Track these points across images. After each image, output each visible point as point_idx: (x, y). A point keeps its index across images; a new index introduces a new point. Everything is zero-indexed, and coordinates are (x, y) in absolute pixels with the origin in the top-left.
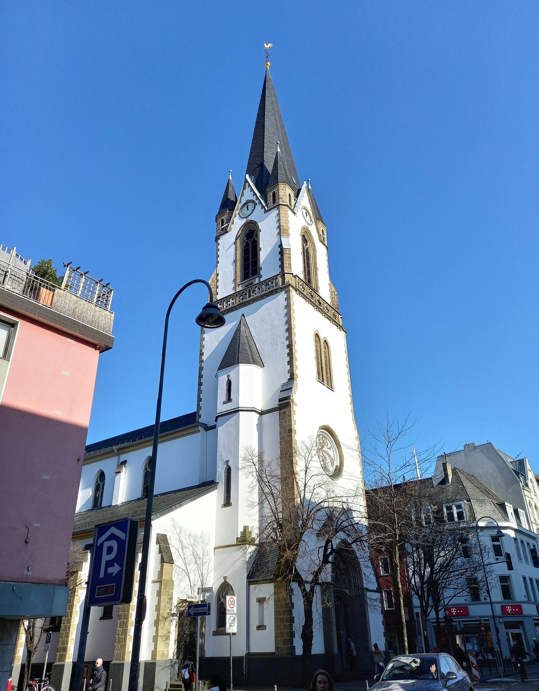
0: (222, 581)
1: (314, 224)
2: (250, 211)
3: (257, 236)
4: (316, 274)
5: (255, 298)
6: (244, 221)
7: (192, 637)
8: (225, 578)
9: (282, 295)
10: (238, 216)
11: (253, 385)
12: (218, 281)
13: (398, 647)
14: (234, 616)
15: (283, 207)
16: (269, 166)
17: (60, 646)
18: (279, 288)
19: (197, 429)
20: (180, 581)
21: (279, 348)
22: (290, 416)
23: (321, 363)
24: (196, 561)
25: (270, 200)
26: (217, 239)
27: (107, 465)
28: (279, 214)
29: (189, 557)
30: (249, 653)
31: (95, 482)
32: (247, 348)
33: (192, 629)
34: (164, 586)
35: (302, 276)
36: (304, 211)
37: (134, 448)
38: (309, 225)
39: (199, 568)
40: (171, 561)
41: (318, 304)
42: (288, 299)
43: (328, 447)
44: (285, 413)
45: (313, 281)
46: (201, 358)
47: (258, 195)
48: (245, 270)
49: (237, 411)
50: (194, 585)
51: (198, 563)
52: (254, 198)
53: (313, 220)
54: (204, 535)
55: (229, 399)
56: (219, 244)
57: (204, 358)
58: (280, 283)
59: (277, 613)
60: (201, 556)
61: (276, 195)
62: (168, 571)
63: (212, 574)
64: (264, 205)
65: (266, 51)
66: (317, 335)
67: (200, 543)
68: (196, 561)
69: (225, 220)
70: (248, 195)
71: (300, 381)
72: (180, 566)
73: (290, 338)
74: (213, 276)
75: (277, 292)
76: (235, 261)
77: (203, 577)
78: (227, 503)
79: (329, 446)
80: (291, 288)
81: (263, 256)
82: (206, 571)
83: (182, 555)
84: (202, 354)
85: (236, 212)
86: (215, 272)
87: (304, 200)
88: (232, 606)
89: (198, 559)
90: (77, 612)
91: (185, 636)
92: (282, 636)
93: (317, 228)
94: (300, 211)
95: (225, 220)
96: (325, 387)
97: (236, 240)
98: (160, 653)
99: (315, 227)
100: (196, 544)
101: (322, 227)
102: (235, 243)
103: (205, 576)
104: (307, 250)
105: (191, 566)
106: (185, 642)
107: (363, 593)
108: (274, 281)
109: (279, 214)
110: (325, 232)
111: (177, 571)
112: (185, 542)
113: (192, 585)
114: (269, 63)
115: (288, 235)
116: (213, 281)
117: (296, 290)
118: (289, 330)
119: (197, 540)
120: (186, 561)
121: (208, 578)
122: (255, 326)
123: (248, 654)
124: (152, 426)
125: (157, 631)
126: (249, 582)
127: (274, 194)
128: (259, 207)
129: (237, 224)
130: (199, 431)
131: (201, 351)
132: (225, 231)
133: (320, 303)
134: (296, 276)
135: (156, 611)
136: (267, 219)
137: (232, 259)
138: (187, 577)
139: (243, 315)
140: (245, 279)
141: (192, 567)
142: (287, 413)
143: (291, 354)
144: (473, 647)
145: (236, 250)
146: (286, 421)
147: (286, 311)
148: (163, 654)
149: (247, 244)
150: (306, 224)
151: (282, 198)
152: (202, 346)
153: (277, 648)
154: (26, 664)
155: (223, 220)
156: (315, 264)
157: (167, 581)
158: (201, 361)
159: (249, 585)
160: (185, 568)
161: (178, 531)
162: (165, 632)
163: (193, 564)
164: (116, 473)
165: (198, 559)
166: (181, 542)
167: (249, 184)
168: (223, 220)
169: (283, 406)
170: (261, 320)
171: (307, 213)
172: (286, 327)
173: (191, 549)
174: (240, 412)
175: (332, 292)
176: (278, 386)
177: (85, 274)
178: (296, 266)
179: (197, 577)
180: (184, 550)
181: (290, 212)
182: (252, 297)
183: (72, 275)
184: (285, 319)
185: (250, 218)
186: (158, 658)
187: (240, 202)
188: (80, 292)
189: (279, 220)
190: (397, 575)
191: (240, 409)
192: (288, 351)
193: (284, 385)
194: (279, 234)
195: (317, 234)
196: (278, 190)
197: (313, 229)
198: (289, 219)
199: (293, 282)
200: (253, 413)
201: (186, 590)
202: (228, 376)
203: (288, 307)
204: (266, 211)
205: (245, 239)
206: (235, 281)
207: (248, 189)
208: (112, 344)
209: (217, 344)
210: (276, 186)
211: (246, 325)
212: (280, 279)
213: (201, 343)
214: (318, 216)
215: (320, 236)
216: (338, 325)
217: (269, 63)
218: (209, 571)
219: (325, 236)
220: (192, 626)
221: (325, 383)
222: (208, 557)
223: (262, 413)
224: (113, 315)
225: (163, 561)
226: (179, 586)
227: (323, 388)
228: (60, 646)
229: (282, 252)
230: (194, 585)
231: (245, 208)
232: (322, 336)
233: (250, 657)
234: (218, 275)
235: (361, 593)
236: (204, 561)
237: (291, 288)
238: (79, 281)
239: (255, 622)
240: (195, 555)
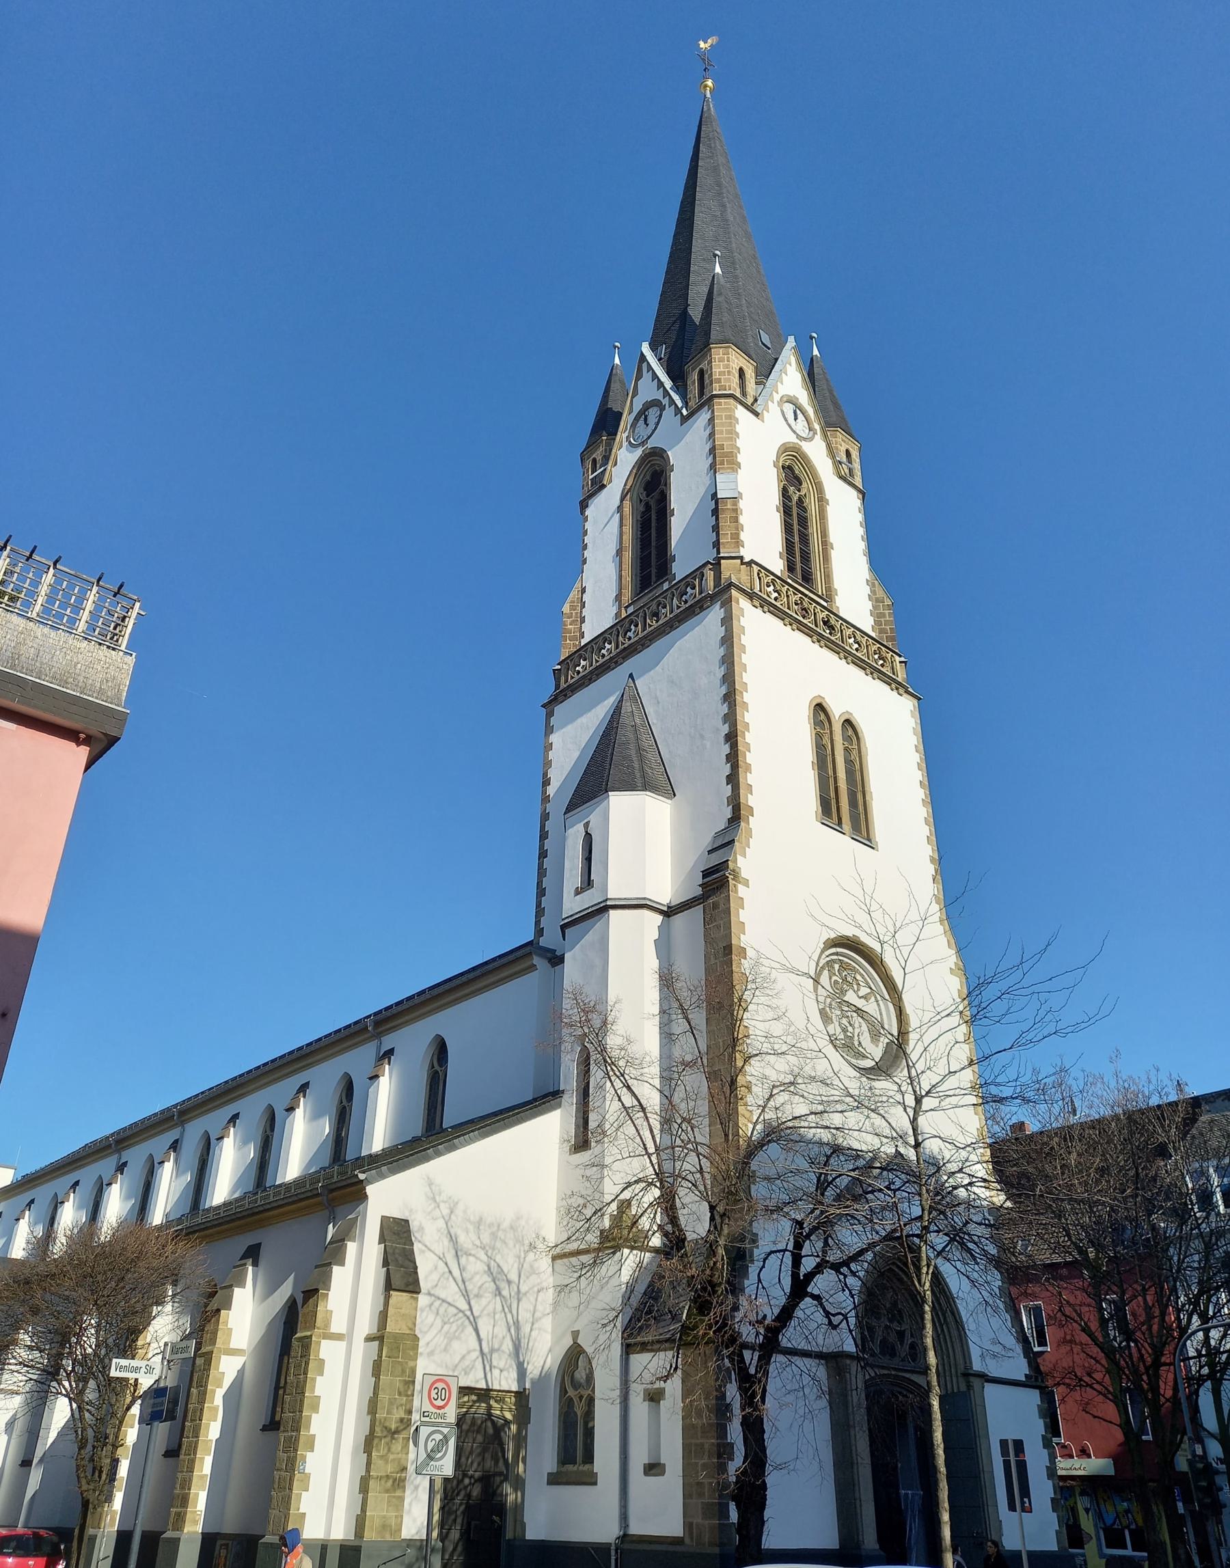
0: (568, 1342)
1: (818, 437)
2: (652, 426)
3: (667, 484)
4: (826, 558)
5: (657, 629)
6: (639, 452)
7: (490, 1484)
8: (576, 1334)
9: (715, 613)
10: (625, 444)
11: (644, 843)
12: (583, 605)
13: (1168, 1542)
14: (445, 1431)
15: (722, 400)
16: (696, 313)
17: (177, 1491)
18: (706, 597)
19: (529, 963)
20: (451, 1340)
21: (708, 744)
22: (728, 911)
23: (835, 778)
24: (498, 1289)
25: (693, 389)
26: (584, 505)
27: (356, 1060)
28: (711, 421)
29: (477, 1278)
30: (625, 1535)
31: (336, 1102)
32: (633, 752)
33: (489, 1464)
34: (390, 1349)
35: (777, 566)
36: (789, 409)
37: (407, 1018)
38: (805, 439)
39: (507, 1308)
40: (412, 1287)
41: (828, 630)
42: (727, 621)
43: (861, 994)
44: (715, 906)
45: (818, 576)
46: (544, 792)
47: (668, 384)
48: (642, 570)
49: (602, 910)
50: (492, 1351)
51: (505, 1293)
52: (659, 395)
53: (817, 427)
54: (523, 1222)
55: (588, 883)
56: (586, 519)
57: (551, 790)
58: (711, 583)
59: (688, 1430)
60: (513, 1276)
61: (706, 376)
62: (403, 1311)
63: (547, 1323)
64: (680, 404)
65: (703, 56)
66: (820, 708)
67: (511, 1243)
68: (498, 1289)
69: (599, 458)
70: (647, 391)
71: (757, 824)
72: (449, 1300)
73: (731, 718)
74: (574, 594)
75: (702, 609)
76: (619, 553)
77: (518, 1328)
78: (582, 1142)
79: (864, 991)
80: (734, 593)
81: (677, 526)
82: (529, 1315)
83: (456, 1273)
84: (546, 782)
85: (622, 435)
86: (578, 585)
87: (790, 379)
88: (439, 1403)
89: (503, 1285)
90: (216, 1409)
91: (467, 1481)
92: (701, 1495)
93: (829, 446)
94: (774, 408)
95: (599, 458)
96: (847, 839)
97: (622, 500)
98: (377, 1522)
99: (824, 444)
100: (498, 1244)
101: (843, 443)
102: (620, 509)
103: (526, 1329)
105: (484, 1301)
106: (469, 1496)
107: (969, 1387)
108: (697, 583)
109: (711, 421)
110: (855, 455)
111: (442, 1311)
112: (464, 1240)
113: (486, 1350)
114: (709, 83)
115: (735, 466)
116: (572, 608)
117: (751, 596)
118: (730, 697)
119: (500, 1234)
120: (469, 1287)
121: (533, 1333)
122: (656, 698)
123: (625, 1537)
125: (369, 1464)
126: (628, 1346)
127: (702, 373)
128: (669, 412)
129: (624, 461)
130: (533, 968)
131: (545, 774)
132: (598, 486)
133: (832, 628)
134: (752, 561)
135: (368, 1413)
136: (688, 438)
137: (613, 547)
138: (470, 1330)
139: (631, 676)
140: (643, 588)
141: (485, 1305)
142: (722, 906)
143: (733, 758)
145: (621, 525)
146: (718, 927)
147: (722, 652)
148: (385, 1527)
149: (648, 507)
150: (792, 439)
151: (719, 381)
152: (548, 764)
153: (688, 1526)
155: (594, 461)
156: (824, 534)
157: (397, 1337)
158: (546, 799)
159: (628, 1354)
160: (465, 1307)
161: (446, 1212)
162: (390, 1469)
163: (488, 1296)
164: (371, 1078)
165: (503, 1285)
166: (453, 1239)
167: (650, 368)
168: (594, 461)
169: (714, 885)
170: (668, 681)
171: (798, 408)
172: (724, 690)
173: (484, 1258)
174: (611, 912)
175: (877, 600)
176: (706, 841)
177: (55, 564)
179: (501, 1330)
180: (463, 1260)
181: (741, 412)
182: (648, 629)
183: (18, 569)
184: (720, 672)
185: (649, 445)
186: (370, 1535)
187: (631, 411)
188: (38, 608)
189: (712, 435)
190: (924, 1327)
191: (609, 903)
192: (726, 749)
193: (718, 835)
194: (713, 468)
195: (829, 462)
198: (738, 428)
199: (740, 576)
200: (645, 912)
201: (467, 1362)
202: (587, 825)
203: (728, 640)
204: (684, 419)
205: (643, 497)
206: (618, 598)
207: (647, 376)
208: (121, 728)
209: (577, 754)
210: (704, 356)
211: (637, 699)
212: (710, 575)
213: (546, 756)
214: (832, 412)
215: (837, 464)
216: (890, 681)
217: (709, 83)
218: (538, 1314)
219: (857, 466)
220: (488, 1456)
221: (847, 826)
222: (534, 1279)
223: (669, 912)
224: (131, 660)
225: (389, 1286)
226: (445, 1350)
227: (841, 843)
228: (177, 1491)
229: (718, 510)
230: (492, 1351)
231: (641, 422)
232: (837, 711)
233: (626, 1546)
234: (583, 591)
235: (963, 1388)
236: (523, 1288)
237: (734, 593)
238: (36, 583)
239: (639, 1457)
240: (496, 1275)
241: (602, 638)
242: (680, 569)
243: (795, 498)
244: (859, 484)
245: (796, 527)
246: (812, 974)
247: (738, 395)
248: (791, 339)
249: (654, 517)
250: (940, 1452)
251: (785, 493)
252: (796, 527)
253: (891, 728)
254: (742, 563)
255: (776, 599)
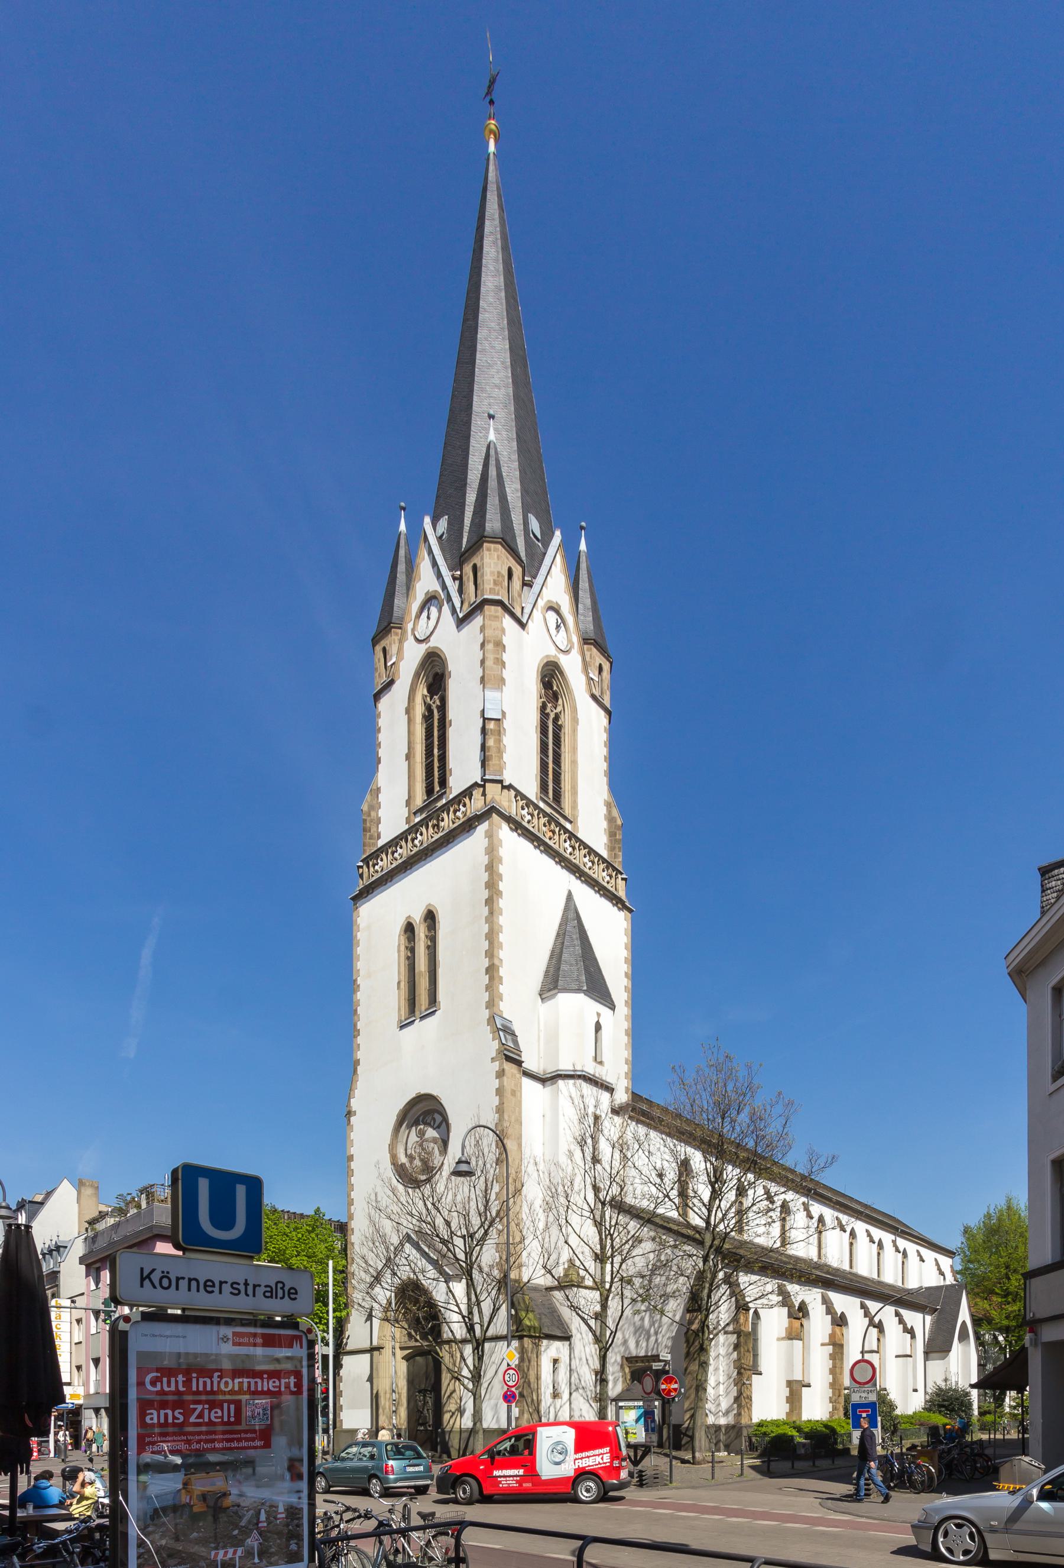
4: (574, 731)
35: (531, 790)
42: (492, 850)
87: (554, 584)
99: (580, 659)
104: (557, 717)
124: (569, 1478)
127: (475, 569)
144: (319, 1533)
150: (552, 652)
154: (436, 1521)
178: (521, 766)
181: (508, 621)
195: (583, 679)
196: (482, 559)
197: (572, 666)
241: (394, 843)
242: (457, 784)
243: (552, 716)
244: (607, 702)
245: (551, 765)
246: (531, 1091)
247: (506, 602)
248: (558, 533)
249: (436, 743)
250: (740, 1520)
251: (543, 708)
252: (551, 765)
253: (610, 933)
254: (504, 787)
255: (529, 822)
